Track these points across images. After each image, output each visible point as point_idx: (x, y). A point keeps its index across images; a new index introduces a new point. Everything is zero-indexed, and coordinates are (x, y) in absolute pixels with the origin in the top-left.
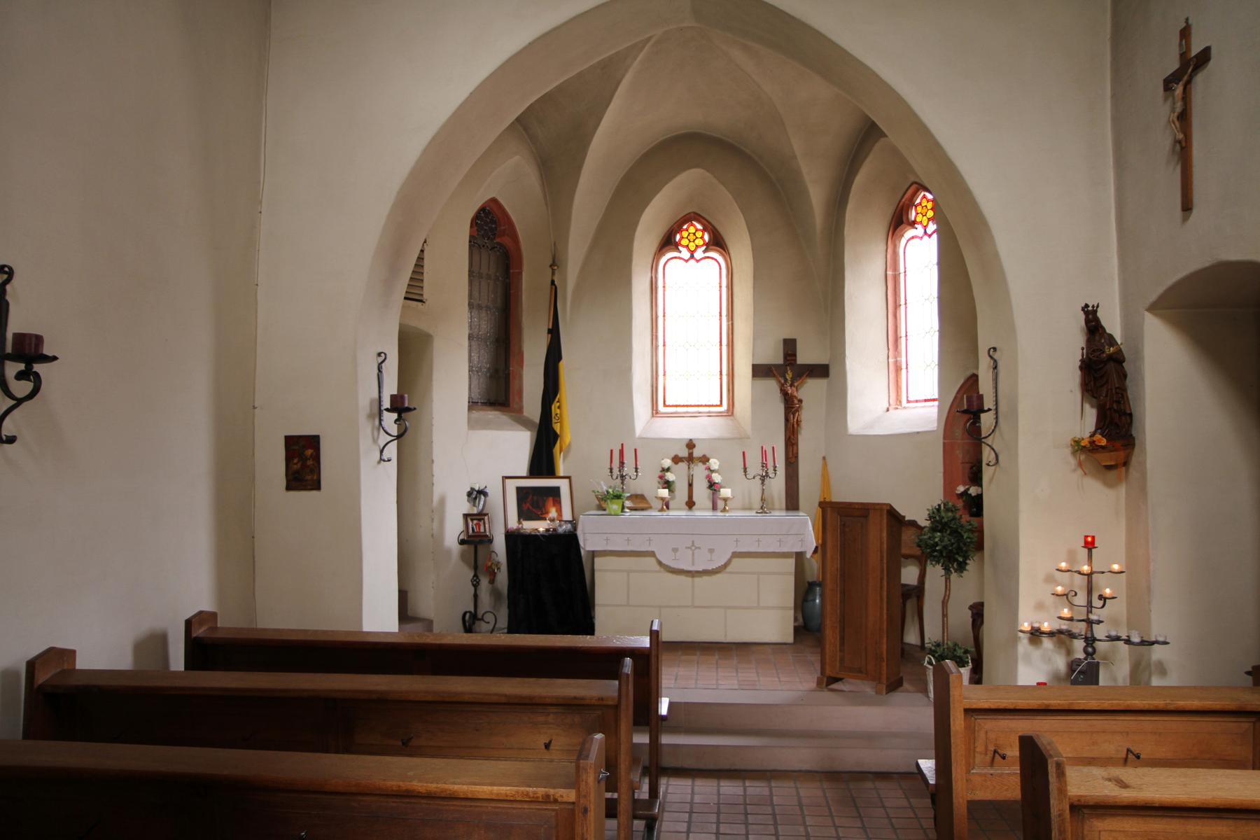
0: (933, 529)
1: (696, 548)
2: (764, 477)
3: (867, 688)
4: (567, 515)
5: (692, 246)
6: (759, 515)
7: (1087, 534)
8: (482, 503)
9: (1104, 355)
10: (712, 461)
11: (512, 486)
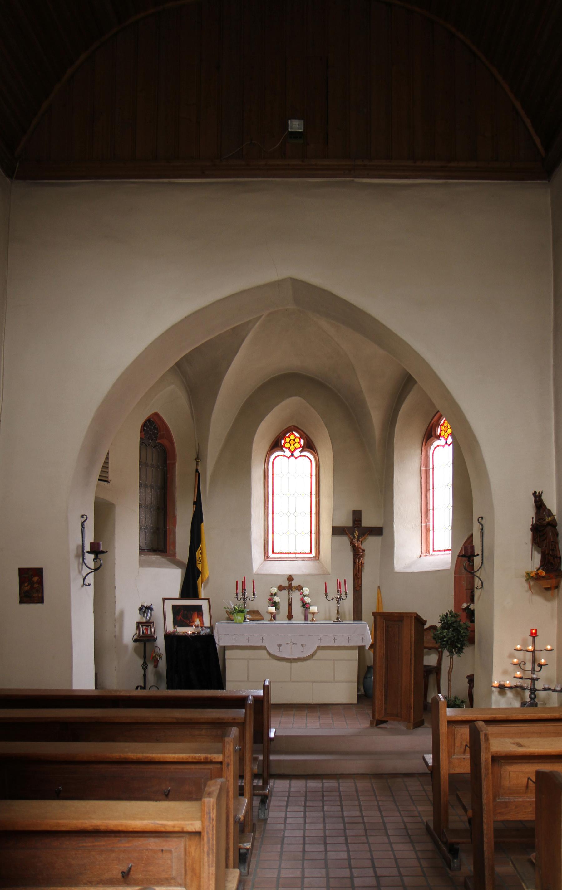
0: (443, 628)
1: (293, 644)
2: (339, 599)
3: (402, 727)
4: (207, 623)
5: (292, 448)
6: (335, 623)
7: (532, 628)
8: (149, 615)
9: (545, 522)
10: (304, 589)
11: (169, 605)
